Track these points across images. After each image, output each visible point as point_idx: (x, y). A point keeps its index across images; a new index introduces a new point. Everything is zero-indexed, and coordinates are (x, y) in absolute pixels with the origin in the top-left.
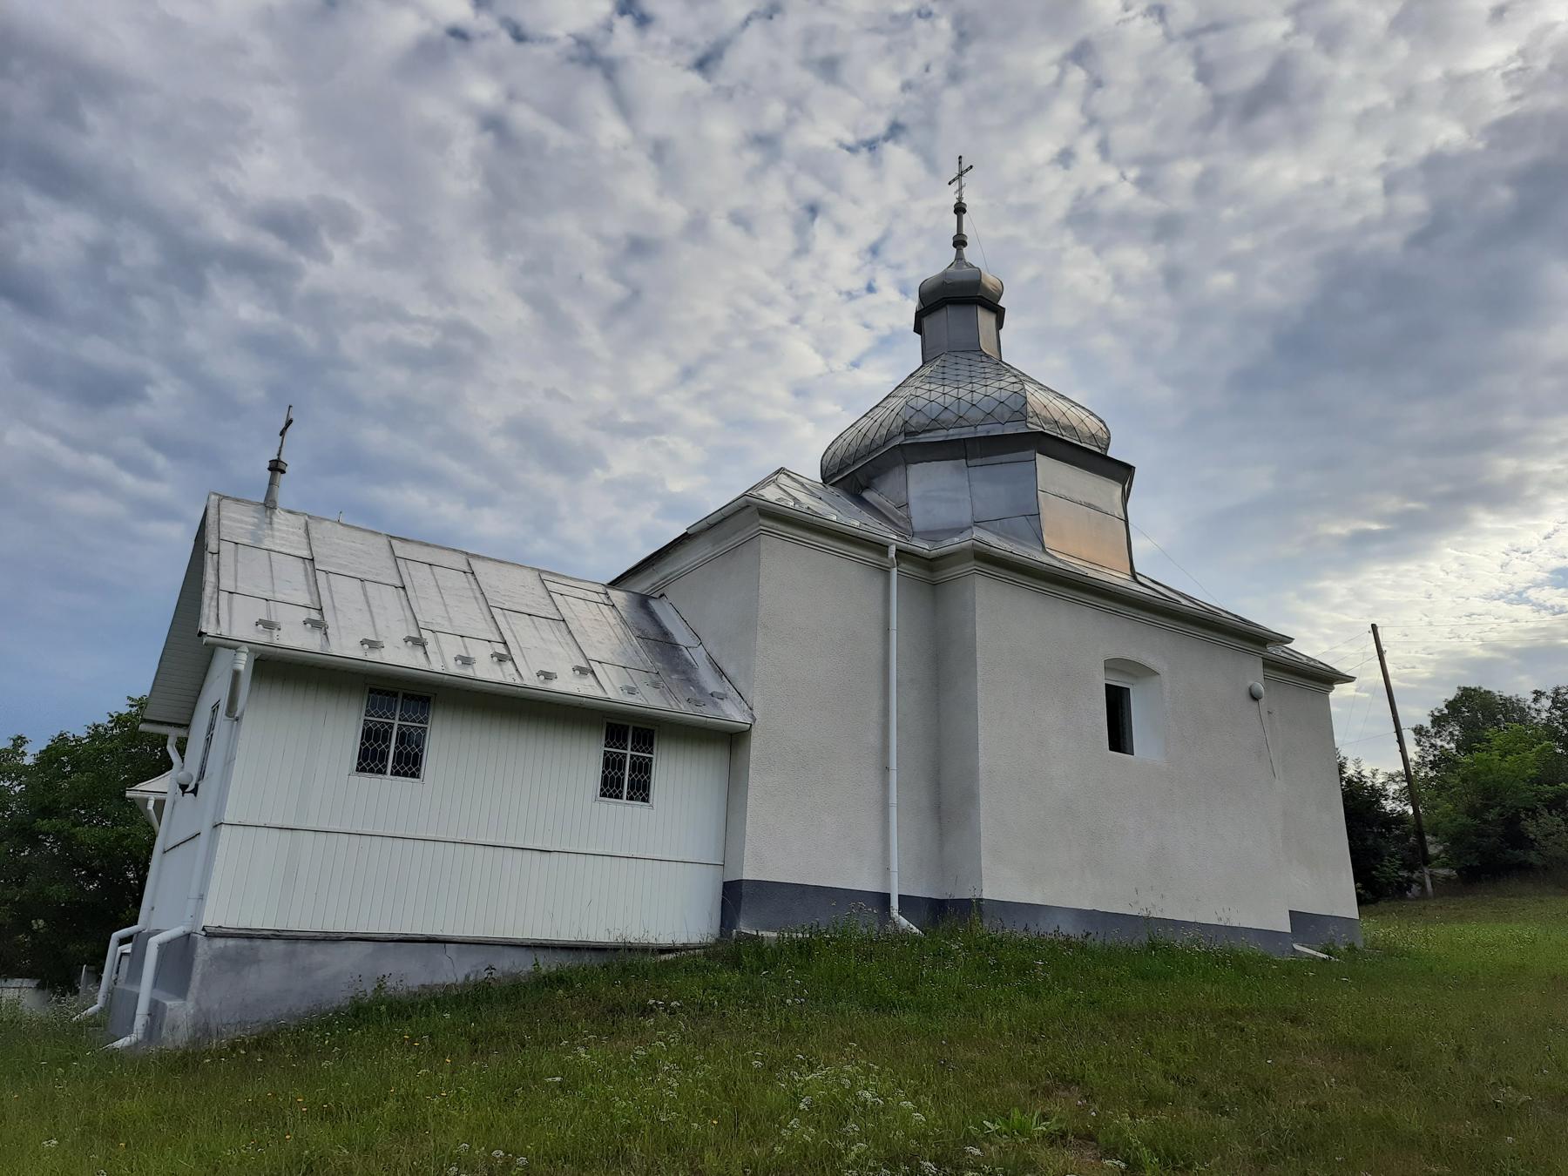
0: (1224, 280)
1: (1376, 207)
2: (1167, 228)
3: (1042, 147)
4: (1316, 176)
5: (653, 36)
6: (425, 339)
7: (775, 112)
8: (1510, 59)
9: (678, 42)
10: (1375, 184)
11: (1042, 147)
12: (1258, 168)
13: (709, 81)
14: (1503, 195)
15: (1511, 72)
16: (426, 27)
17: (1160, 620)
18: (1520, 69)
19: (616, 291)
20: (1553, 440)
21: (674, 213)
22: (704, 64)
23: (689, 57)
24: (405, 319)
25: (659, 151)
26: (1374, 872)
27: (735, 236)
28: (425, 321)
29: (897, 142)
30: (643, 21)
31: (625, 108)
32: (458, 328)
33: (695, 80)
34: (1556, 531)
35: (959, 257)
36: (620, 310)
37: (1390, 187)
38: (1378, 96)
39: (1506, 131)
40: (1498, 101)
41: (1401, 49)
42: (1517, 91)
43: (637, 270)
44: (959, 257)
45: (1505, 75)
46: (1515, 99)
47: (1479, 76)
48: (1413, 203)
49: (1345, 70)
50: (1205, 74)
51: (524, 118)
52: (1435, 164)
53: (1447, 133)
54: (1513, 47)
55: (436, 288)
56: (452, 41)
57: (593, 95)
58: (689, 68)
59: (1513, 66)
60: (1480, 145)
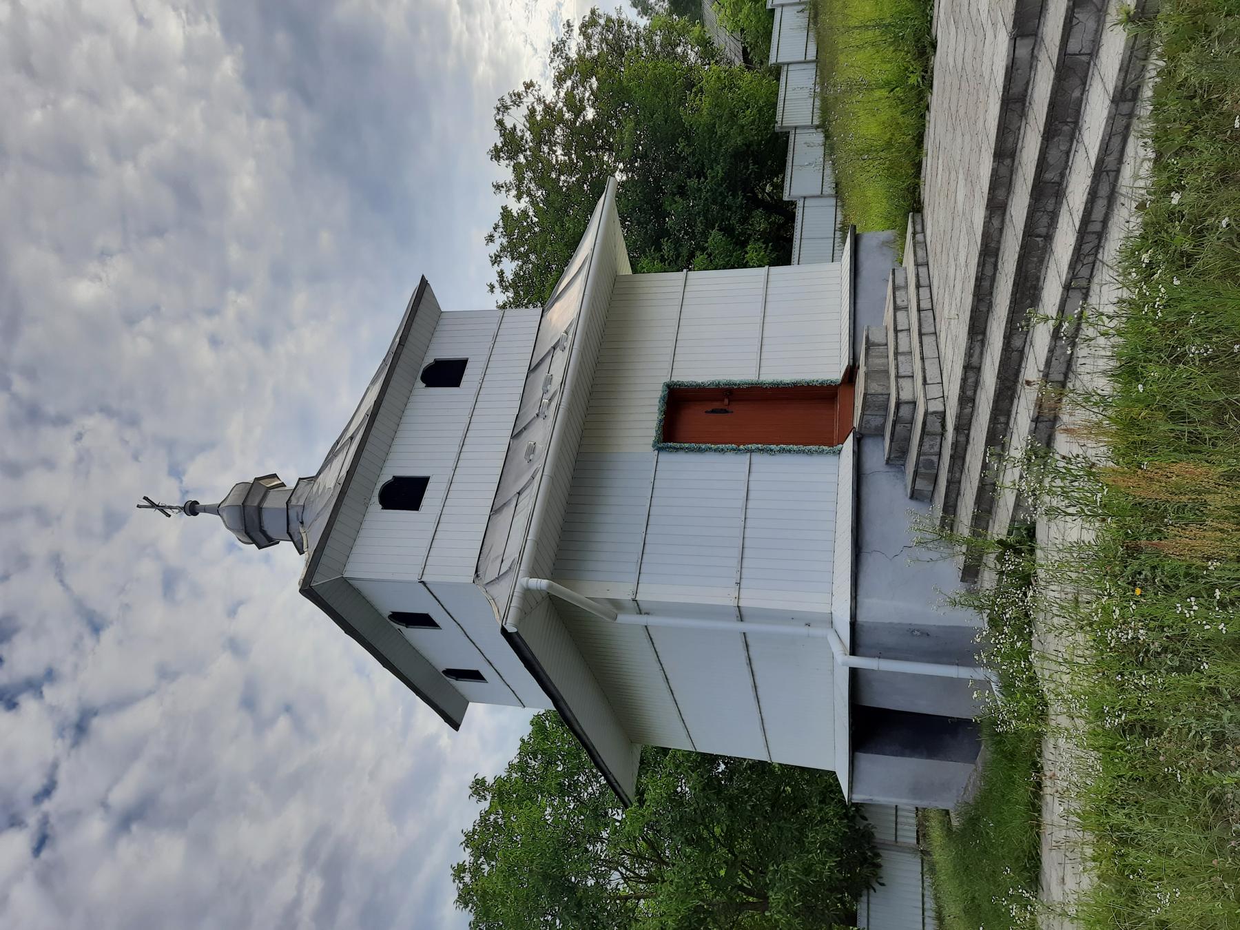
0: (325, 237)
1: (280, 127)
2: (280, 276)
3: (205, 357)
4: (250, 164)
5: (65, 668)
6: (315, 886)
7: (148, 568)
8: (179, 16)
9: (76, 646)
10: (262, 124)
11: (205, 357)
12: (240, 206)
13: (111, 623)
14: (282, 40)
15: (188, 19)
16: (29, 877)
17: (545, 679)
18: (187, 12)
19: (283, 723)
20: (466, 35)
21: (224, 664)
22: (96, 628)
23: (88, 641)
24: (296, 903)
25: (166, 674)
26: (578, 124)
27: (245, 614)
28: (302, 880)
29: (184, 473)
30: (50, 675)
31: (122, 703)
32: (310, 856)
33: (107, 636)
34: (532, 45)
35: (215, 510)
36: (299, 725)
37: (266, 115)
38: (196, 112)
39: (231, 28)
40: (208, 29)
41: (160, 91)
42: (203, 18)
43: (267, 705)
44: (215, 510)
45: (189, 24)
46: (208, 19)
47: (188, 39)
48: (279, 100)
49: (172, 130)
50: (158, 231)
51: (123, 794)
52: (250, 80)
53: (228, 67)
54: (171, 14)
55: (272, 869)
56: (45, 854)
57: (106, 728)
58: (98, 641)
59: (184, 15)
60: (240, 48)
